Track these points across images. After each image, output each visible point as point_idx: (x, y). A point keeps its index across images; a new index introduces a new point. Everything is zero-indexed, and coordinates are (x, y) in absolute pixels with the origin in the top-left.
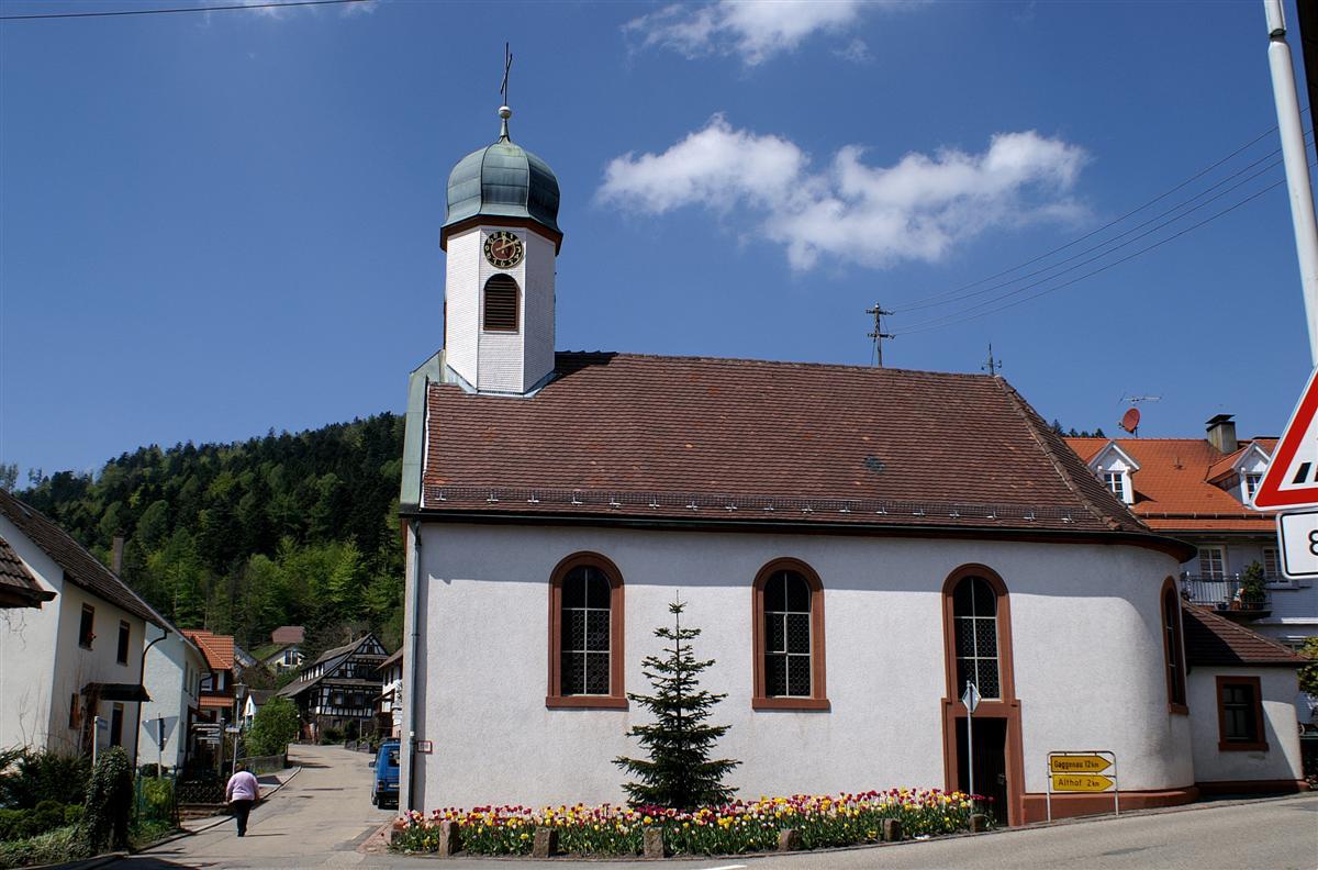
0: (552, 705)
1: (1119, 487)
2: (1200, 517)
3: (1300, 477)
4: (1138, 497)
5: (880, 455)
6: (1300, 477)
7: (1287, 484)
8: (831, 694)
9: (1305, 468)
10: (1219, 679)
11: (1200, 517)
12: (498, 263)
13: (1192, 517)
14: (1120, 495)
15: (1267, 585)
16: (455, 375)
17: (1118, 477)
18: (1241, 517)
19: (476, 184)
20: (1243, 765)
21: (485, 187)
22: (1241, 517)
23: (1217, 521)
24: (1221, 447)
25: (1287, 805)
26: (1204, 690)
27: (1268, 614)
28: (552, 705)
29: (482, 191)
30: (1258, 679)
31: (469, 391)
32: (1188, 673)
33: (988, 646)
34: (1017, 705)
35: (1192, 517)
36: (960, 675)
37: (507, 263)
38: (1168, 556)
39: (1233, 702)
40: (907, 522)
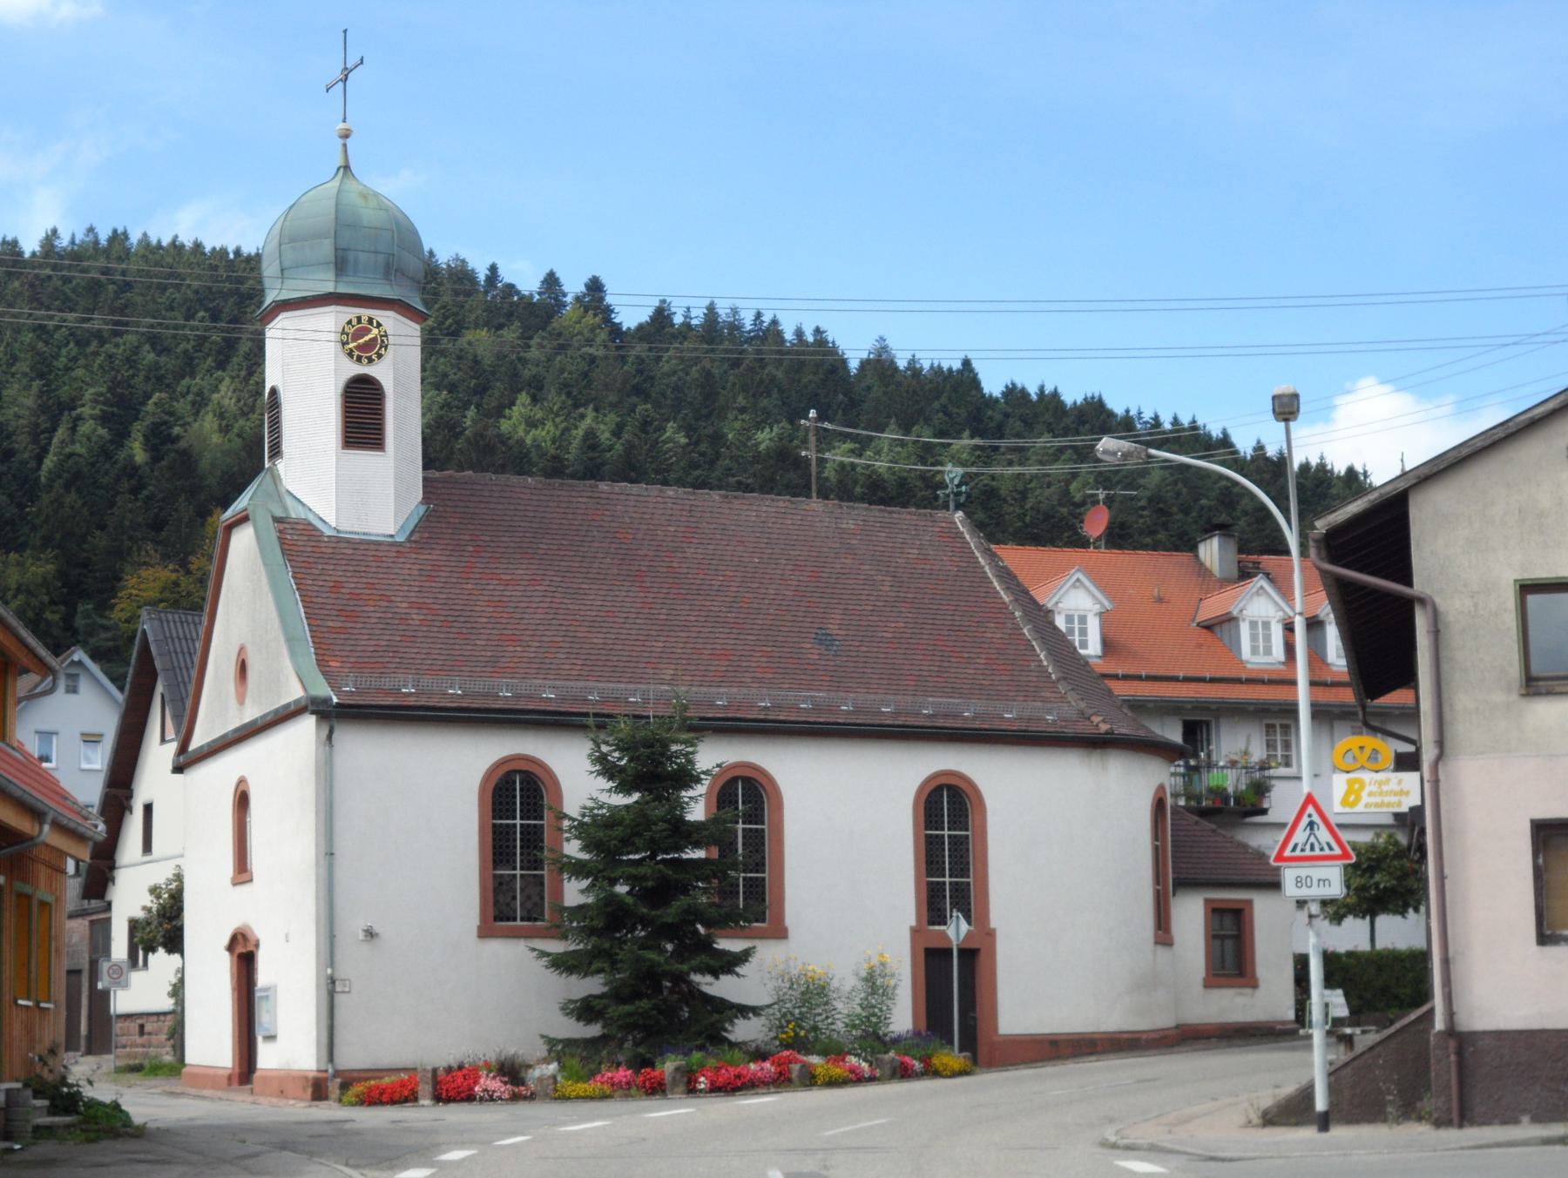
0: (485, 932)
1: (1083, 632)
2: (1187, 680)
3: (1294, 849)
4: (1107, 644)
5: (833, 629)
6: (1294, 849)
7: (1287, 853)
8: (790, 919)
9: (1295, 846)
10: (1207, 901)
11: (1187, 680)
12: (359, 359)
13: (1175, 679)
14: (1084, 645)
15: (1272, 772)
16: (300, 507)
17: (1083, 619)
18: (1238, 681)
19: (326, 249)
20: (1231, 1006)
21: (340, 253)
22: (1238, 681)
23: (1208, 686)
24: (1216, 569)
25: (1223, 956)
26: (1190, 913)
27: (1264, 812)
28: (485, 932)
29: (336, 257)
30: (1250, 903)
31: (328, 532)
32: (1174, 895)
33: (961, 867)
34: (991, 935)
35: (1175, 679)
36: (934, 905)
37: (370, 360)
38: (1161, 760)
39: (1222, 929)
40: (878, 722)
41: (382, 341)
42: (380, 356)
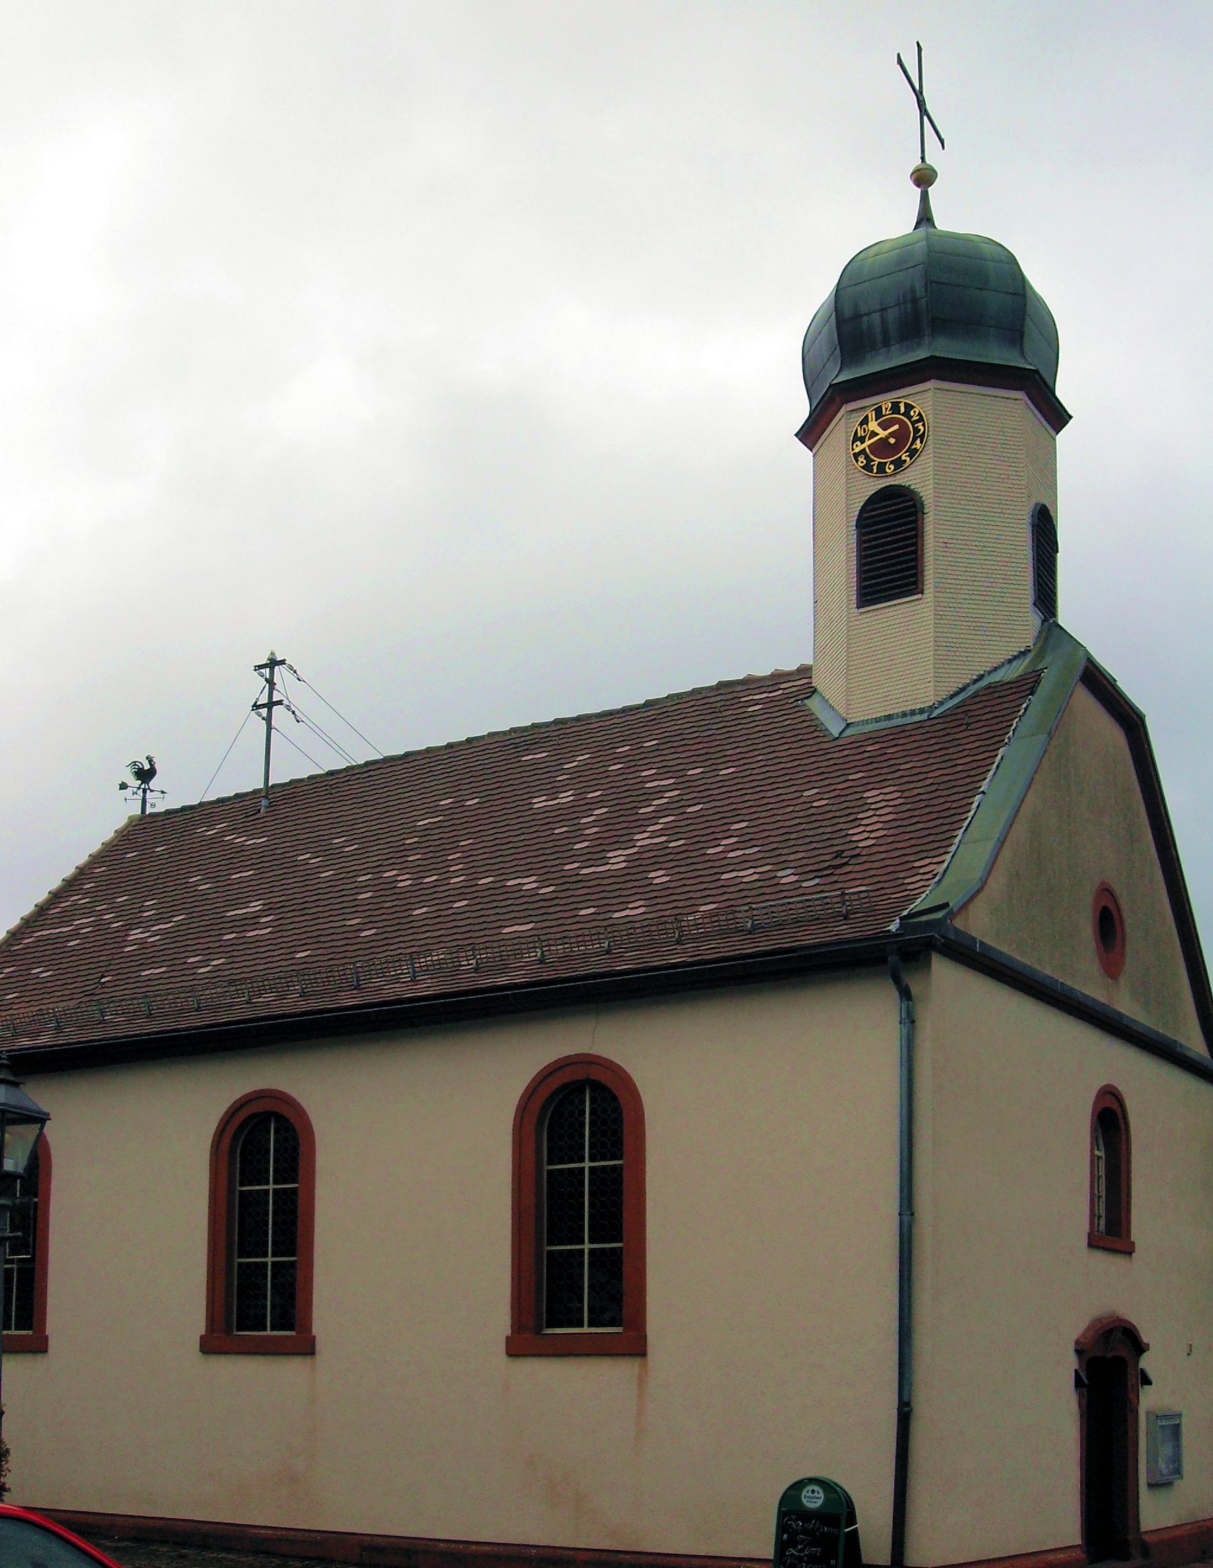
0: (211, 1345)
28: (211, 1345)
37: (899, 464)
41: (916, 430)
42: (913, 453)
